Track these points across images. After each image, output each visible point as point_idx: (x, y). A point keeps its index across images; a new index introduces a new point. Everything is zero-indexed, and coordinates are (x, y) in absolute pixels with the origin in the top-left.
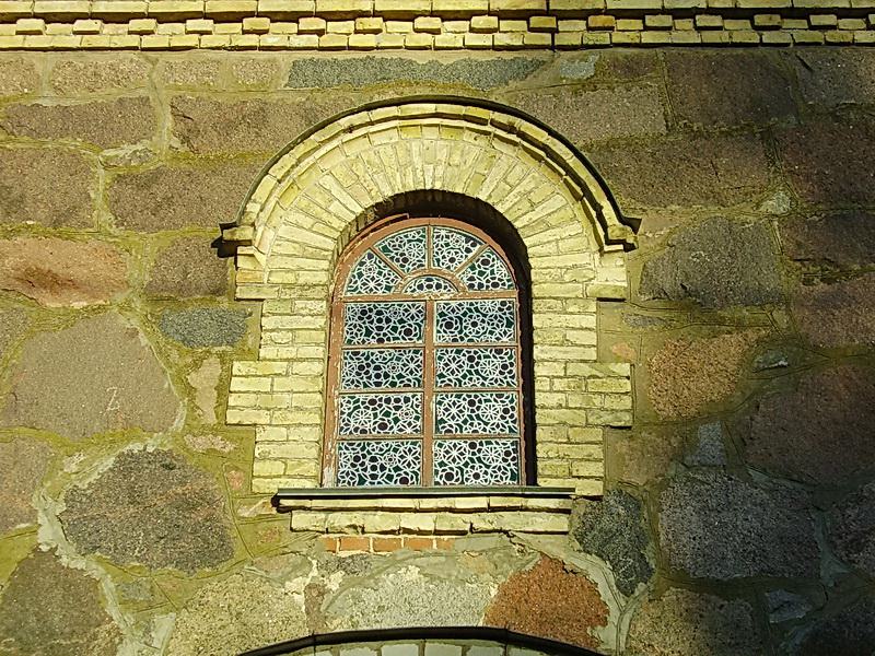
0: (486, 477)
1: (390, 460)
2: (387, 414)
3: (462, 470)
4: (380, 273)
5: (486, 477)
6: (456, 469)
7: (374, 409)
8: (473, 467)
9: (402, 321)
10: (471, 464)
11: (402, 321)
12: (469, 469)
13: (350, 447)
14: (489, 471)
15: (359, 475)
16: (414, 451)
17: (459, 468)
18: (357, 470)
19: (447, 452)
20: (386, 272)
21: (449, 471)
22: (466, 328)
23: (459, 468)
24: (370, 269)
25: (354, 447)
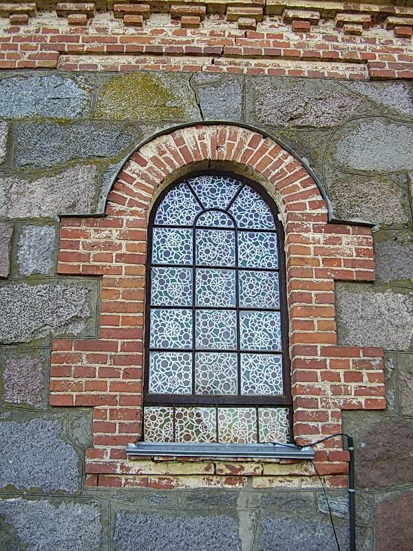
0: (249, 196)
1: (217, 318)
2: (216, 331)
3: (213, 199)
4: (257, 257)
5: (214, 252)
6: (216, 196)
7: (212, 341)
8: (204, 294)
9: (221, 325)
10: (163, 414)
11: (221, 325)
12: (246, 281)
13: (224, 275)
14: (216, 248)
15: (159, 317)
16: (245, 256)
17: (245, 241)
18: (250, 383)
19: (253, 252)
20: (259, 261)
21: (167, 258)
22: (245, 289)
23: (245, 241)
24: (261, 251)
25: (227, 274)
